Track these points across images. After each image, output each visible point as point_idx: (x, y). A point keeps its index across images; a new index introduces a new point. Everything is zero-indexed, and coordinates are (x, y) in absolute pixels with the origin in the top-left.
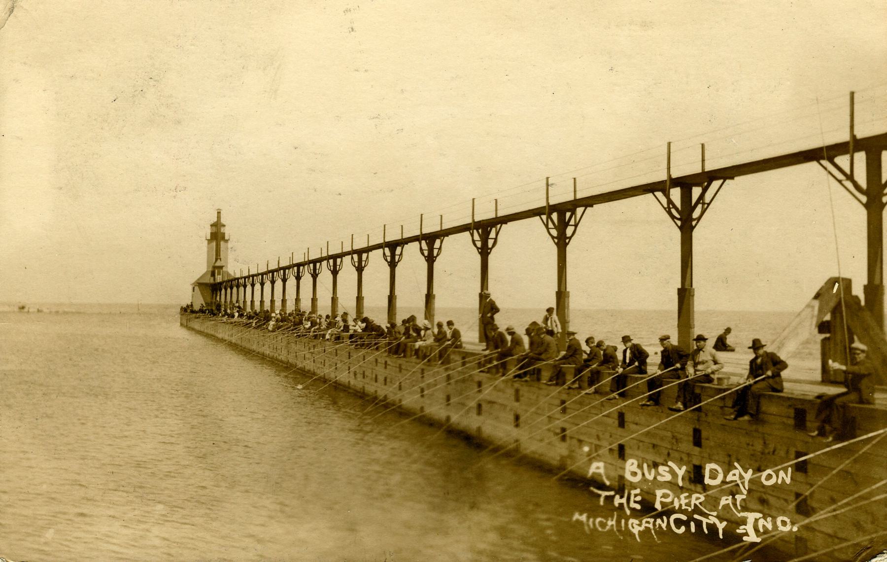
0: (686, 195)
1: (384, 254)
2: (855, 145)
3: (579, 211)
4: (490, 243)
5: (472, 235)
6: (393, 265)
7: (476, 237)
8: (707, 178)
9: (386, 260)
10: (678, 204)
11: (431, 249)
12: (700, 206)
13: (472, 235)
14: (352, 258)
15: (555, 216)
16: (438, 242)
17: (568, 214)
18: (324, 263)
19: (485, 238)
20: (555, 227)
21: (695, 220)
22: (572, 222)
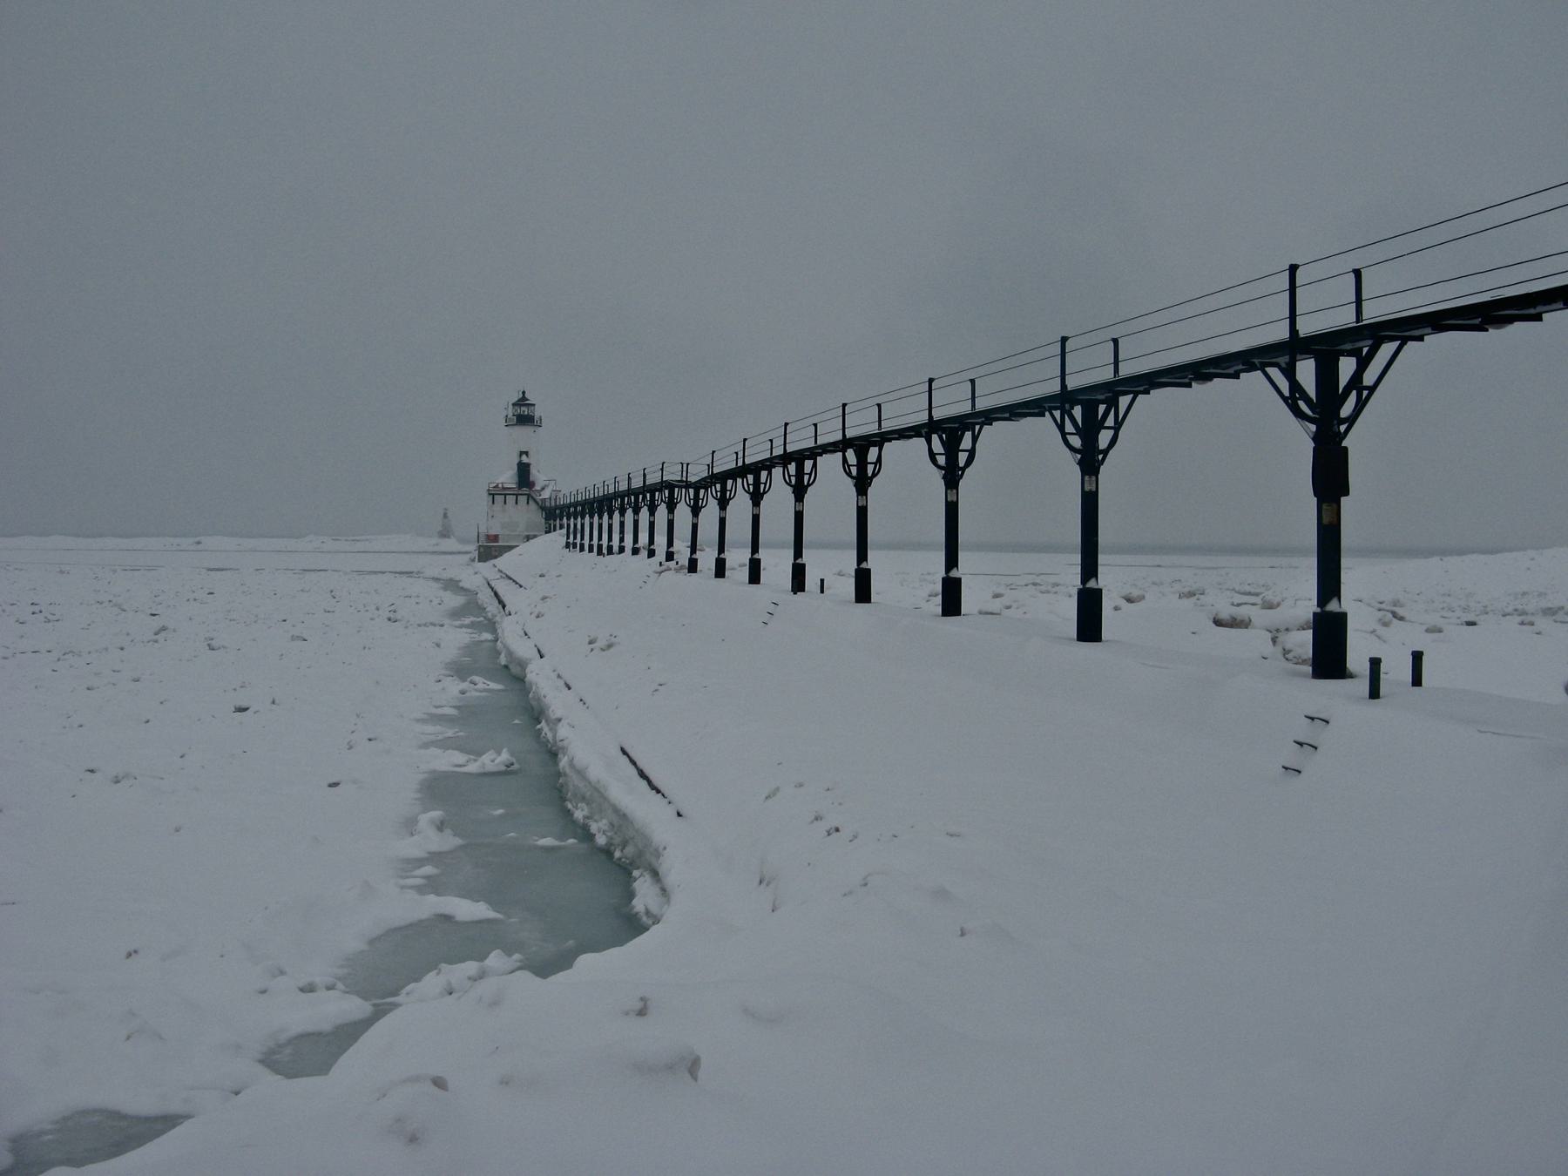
1: (845, 460)
2: (1296, 346)
3: (1124, 401)
4: (962, 458)
5: (929, 442)
7: (937, 446)
9: (849, 474)
10: (1310, 387)
11: (862, 463)
12: (1353, 396)
13: (929, 442)
15: (1077, 412)
17: (1102, 408)
18: (777, 472)
19: (952, 448)
20: (1079, 432)
21: (1343, 421)
22: (1110, 422)
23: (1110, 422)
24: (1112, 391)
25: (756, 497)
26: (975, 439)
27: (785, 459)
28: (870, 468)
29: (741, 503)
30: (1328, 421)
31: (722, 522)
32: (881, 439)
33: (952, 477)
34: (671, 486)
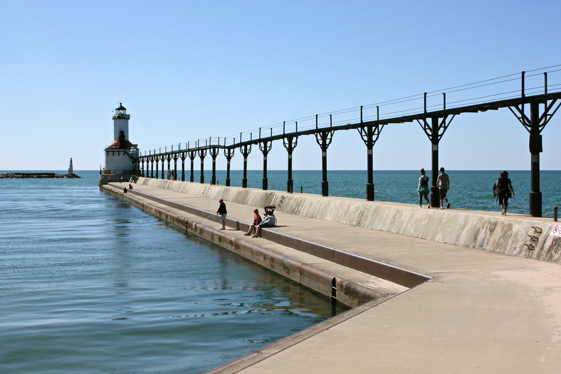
0: (370, 130)
2: (524, 100)
4: (328, 141)
5: (317, 136)
6: (265, 153)
7: (319, 138)
8: (445, 113)
9: (286, 147)
11: (290, 143)
13: (317, 136)
14: (260, 145)
15: (366, 128)
16: (294, 139)
17: (374, 128)
18: (208, 150)
21: (439, 136)
22: (376, 132)
23: (376, 132)
24: (376, 124)
26: (332, 136)
28: (268, 148)
30: (535, 126)
32: (297, 134)
33: (324, 147)
34: (175, 153)
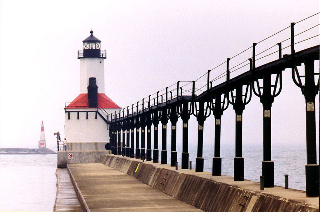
1: (102, 56)
18: (287, 73)
25: (267, 100)
27: (291, 61)
29: (254, 108)
31: (267, 123)
